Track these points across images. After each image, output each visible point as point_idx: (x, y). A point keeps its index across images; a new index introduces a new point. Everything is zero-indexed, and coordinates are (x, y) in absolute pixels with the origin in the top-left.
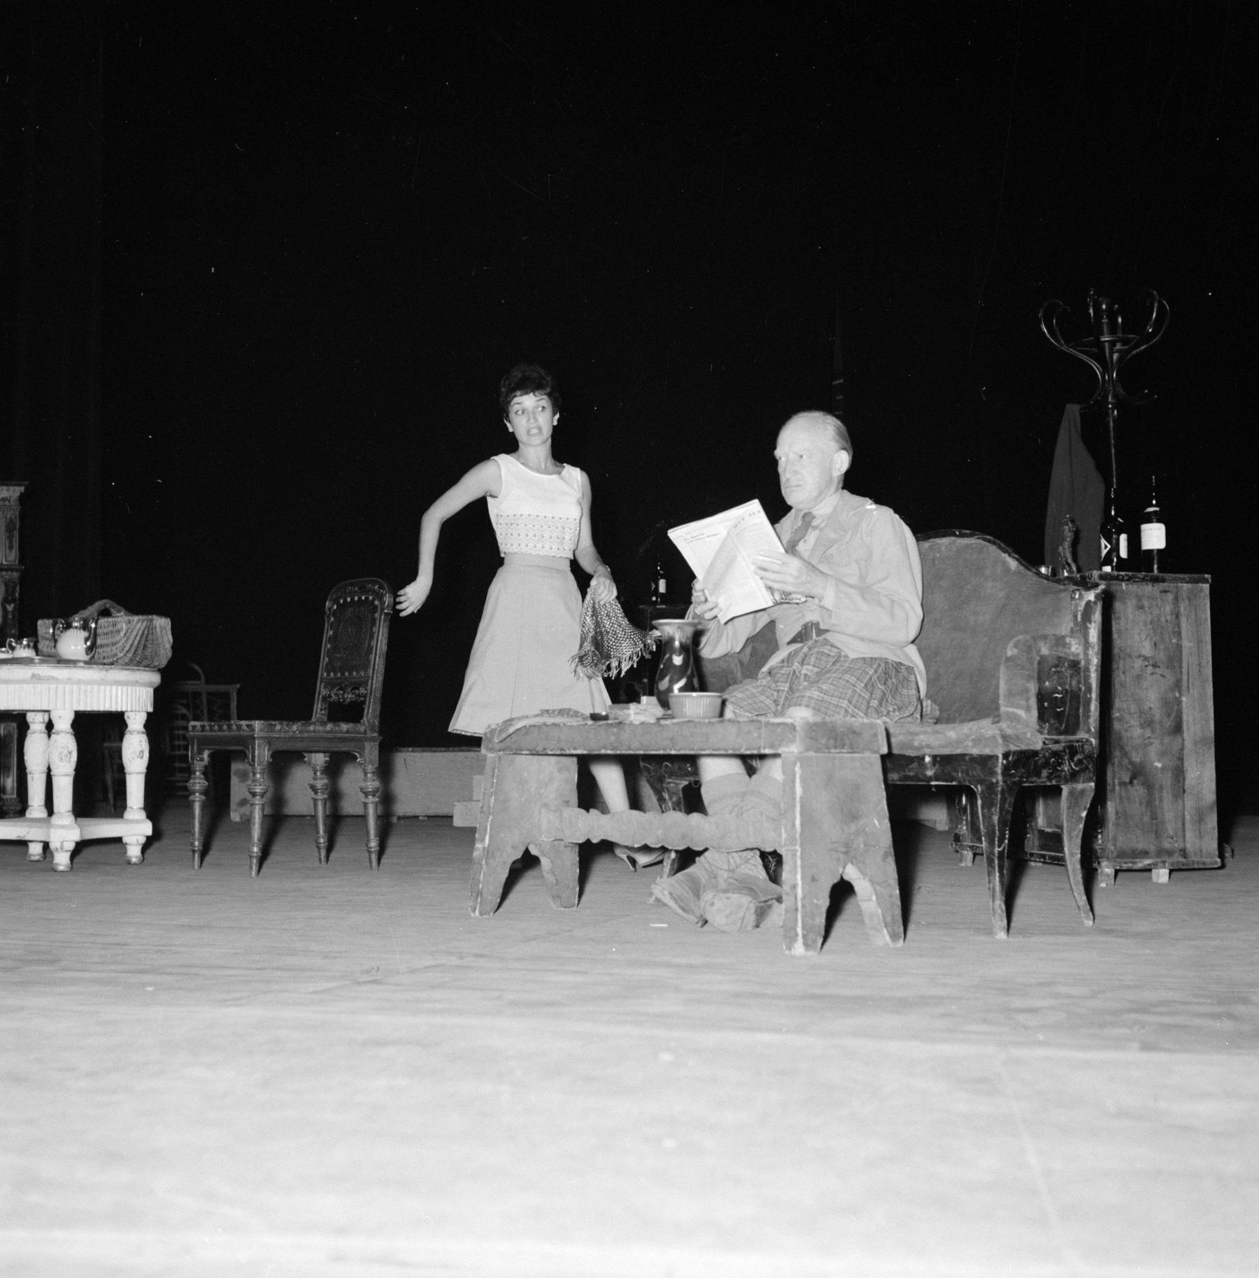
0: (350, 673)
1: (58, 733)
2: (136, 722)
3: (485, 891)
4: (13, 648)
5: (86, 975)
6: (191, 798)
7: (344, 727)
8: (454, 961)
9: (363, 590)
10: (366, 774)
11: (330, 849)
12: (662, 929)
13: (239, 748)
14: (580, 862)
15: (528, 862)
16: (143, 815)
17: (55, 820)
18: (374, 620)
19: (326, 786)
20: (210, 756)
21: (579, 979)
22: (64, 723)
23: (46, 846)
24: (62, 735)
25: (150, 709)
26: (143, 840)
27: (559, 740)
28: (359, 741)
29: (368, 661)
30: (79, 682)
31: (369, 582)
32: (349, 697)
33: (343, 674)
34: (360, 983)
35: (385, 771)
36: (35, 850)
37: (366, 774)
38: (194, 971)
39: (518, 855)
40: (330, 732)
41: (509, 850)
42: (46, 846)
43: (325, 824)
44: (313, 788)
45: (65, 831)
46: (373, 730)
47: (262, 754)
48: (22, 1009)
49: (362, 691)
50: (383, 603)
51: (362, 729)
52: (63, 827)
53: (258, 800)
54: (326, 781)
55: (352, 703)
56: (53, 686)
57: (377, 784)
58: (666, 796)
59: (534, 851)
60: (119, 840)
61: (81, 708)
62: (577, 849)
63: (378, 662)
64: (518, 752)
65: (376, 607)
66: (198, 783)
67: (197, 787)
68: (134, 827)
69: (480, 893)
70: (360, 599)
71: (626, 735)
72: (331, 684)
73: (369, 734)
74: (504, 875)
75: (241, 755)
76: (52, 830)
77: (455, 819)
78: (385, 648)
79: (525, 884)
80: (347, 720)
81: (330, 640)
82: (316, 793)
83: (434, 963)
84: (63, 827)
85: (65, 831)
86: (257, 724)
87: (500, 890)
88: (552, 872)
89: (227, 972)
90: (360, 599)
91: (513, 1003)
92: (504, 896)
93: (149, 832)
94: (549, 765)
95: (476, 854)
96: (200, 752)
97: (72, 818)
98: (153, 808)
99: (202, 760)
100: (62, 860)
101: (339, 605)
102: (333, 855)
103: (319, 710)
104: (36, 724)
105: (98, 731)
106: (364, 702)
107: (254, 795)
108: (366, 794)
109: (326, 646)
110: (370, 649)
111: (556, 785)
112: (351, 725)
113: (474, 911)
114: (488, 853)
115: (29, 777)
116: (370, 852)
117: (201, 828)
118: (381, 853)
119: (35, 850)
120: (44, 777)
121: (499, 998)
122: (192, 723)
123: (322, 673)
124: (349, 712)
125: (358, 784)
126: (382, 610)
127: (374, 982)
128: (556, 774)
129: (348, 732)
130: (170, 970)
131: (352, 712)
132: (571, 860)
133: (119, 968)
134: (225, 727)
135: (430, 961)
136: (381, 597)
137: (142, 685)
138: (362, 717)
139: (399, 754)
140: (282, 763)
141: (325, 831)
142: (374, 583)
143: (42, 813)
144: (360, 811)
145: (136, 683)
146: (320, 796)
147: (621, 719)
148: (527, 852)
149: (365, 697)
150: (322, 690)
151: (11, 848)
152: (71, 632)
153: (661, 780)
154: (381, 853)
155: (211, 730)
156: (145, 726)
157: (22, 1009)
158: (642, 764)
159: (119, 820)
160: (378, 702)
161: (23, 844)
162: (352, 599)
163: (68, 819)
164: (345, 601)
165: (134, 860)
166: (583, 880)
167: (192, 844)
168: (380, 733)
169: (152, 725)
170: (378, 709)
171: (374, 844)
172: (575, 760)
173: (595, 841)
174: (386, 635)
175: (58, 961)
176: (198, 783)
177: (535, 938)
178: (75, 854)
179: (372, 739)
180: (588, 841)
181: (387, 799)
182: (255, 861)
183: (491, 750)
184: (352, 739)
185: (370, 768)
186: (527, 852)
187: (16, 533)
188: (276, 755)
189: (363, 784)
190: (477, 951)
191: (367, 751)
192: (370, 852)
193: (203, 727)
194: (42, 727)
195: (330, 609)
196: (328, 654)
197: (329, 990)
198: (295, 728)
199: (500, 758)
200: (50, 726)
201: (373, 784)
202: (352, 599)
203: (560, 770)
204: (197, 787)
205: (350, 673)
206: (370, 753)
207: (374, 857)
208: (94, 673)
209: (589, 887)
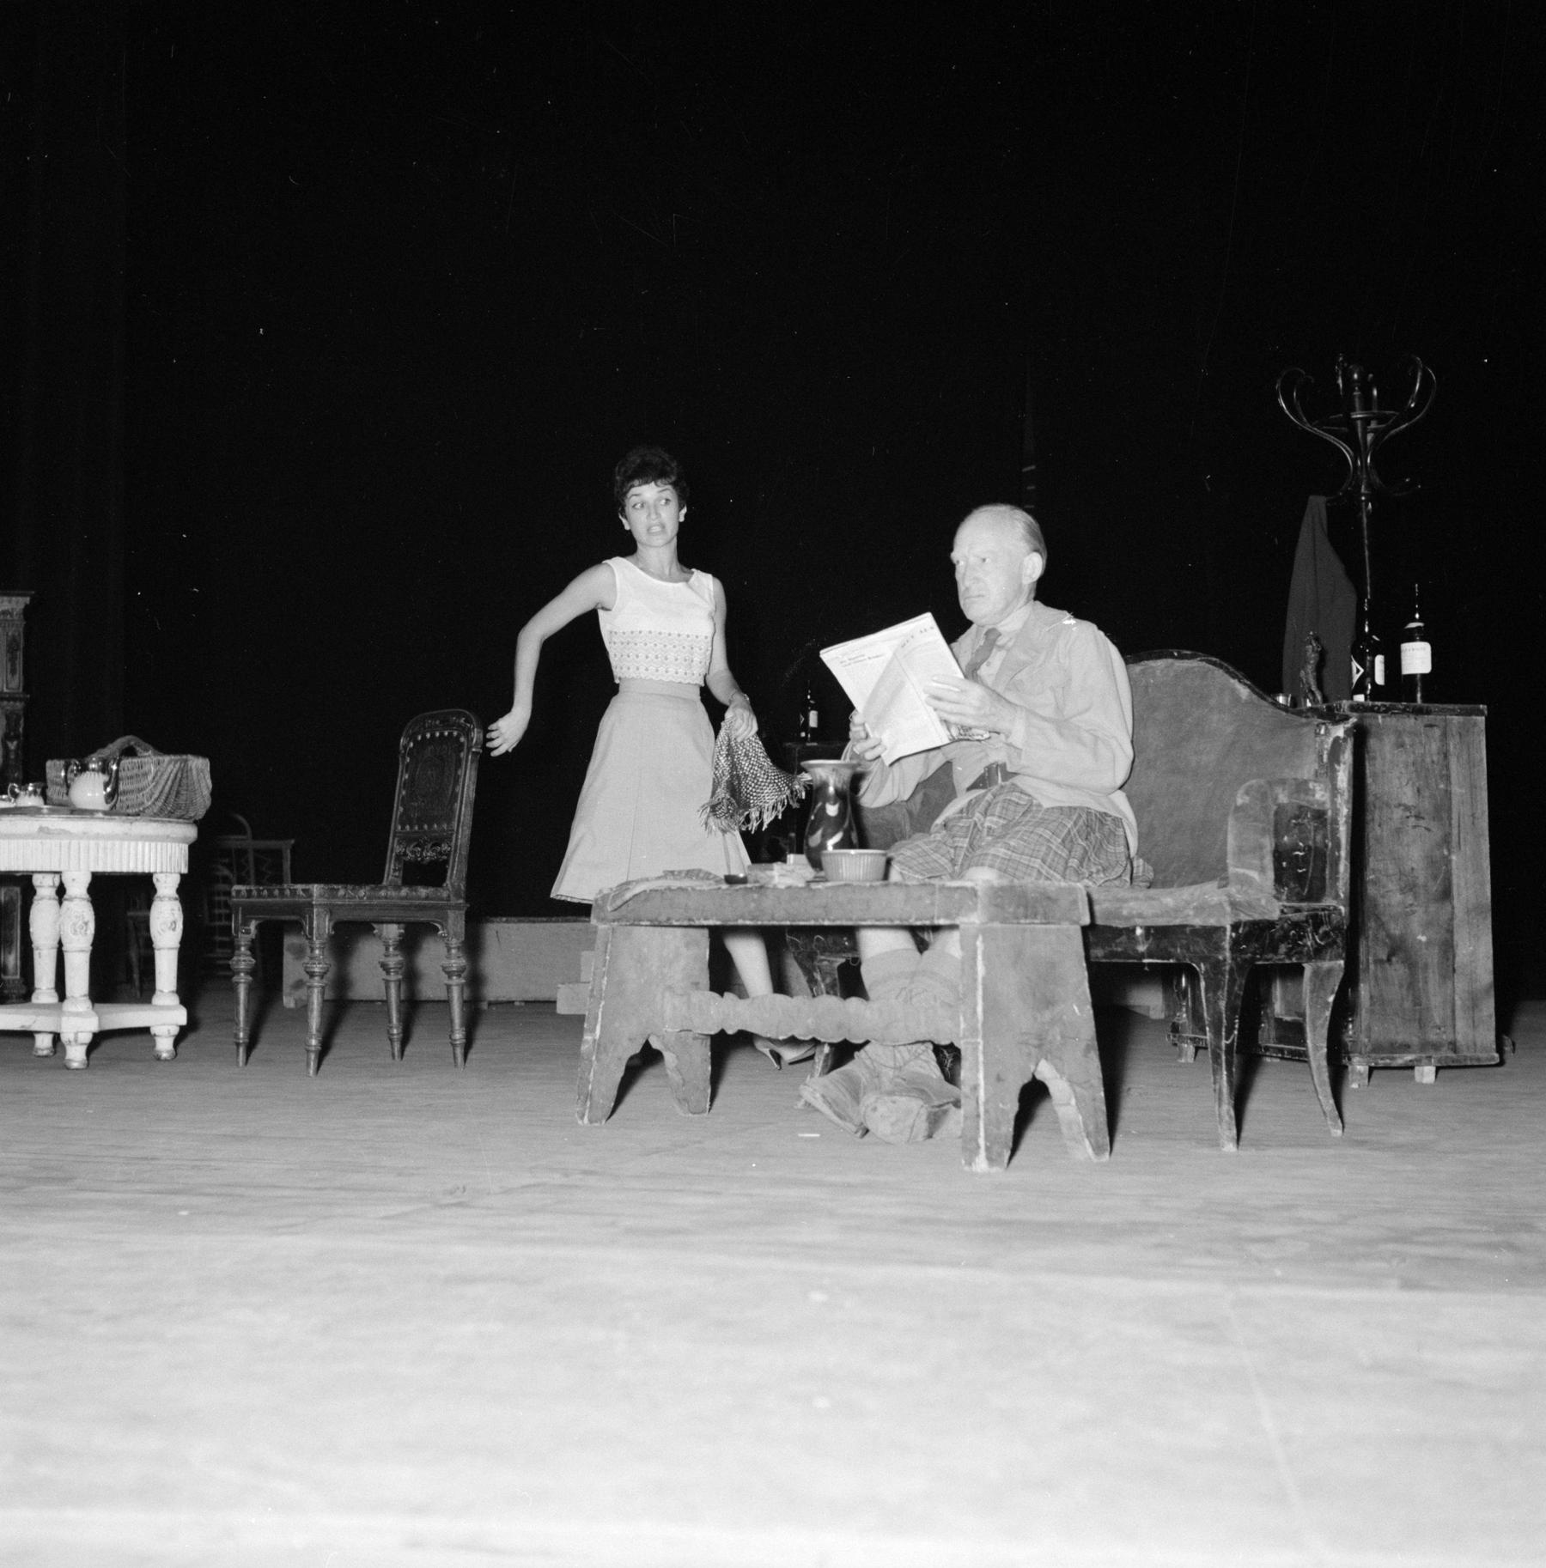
0: (430, 826)
1: (71, 899)
2: (167, 886)
3: (595, 1093)
4: (16, 796)
5: (106, 1196)
6: (235, 979)
7: (423, 891)
8: (557, 1179)
9: (446, 724)
10: (449, 950)
11: (405, 1041)
12: (812, 1139)
13: (294, 918)
14: (713, 1057)
15: (648, 1057)
16: (175, 1000)
17: (67, 1006)
18: (459, 761)
19: (400, 965)
20: (258, 927)
21: (711, 1201)
22: (78, 887)
23: (57, 1038)
24: (76, 901)
25: (185, 870)
26: (175, 1031)
27: (687, 908)
28: (441, 910)
29: (452, 811)
30: (97, 837)
31: (453, 714)
32: (429, 855)
33: (421, 827)
34: (442, 1207)
35: (473, 946)
36: (43, 1043)
37: (449, 950)
38: (239, 1191)
39: (636, 1049)
40: (406, 898)
41: (625, 1043)
42: (57, 1038)
43: (399, 1011)
44: (384, 966)
45: (80, 1020)
46: (458, 896)
47: (322, 925)
48: (27, 1238)
49: (445, 847)
50: (470, 740)
51: (445, 895)
52: (78, 1014)
53: (316, 982)
54: (400, 958)
55: (433, 863)
56: (65, 842)
57: (463, 962)
58: (818, 976)
59: (655, 1044)
60: (146, 1031)
61: (100, 869)
62: (709, 1042)
63: (464, 812)
64: (636, 922)
65: (462, 745)
66: (243, 960)
67: (242, 966)
68: (164, 1015)
69: (589, 1096)
70: (442, 734)
71: (768, 902)
72: (406, 840)
73: (453, 901)
74: (619, 1073)
75: (296, 927)
76: (64, 1019)
77: (559, 1005)
78: (472, 795)
79: (645, 1085)
80: (426, 883)
81: (405, 785)
82: (388, 973)
83: (533, 1181)
84: (78, 1014)
85: (80, 1020)
86: (316, 889)
87: (614, 1093)
88: (678, 1070)
89: (279, 1193)
90: (442, 734)
91: (630, 1231)
92: (619, 1099)
93: (183, 1021)
94: (674, 938)
95: (584, 1048)
96: (246, 923)
97: (89, 1003)
98: (188, 992)
99: (248, 932)
100: (76, 1055)
101: (416, 742)
102: (409, 1049)
103: (391, 871)
104: (45, 888)
105: (120, 897)
106: (447, 862)
107: (312, 975)
108: (450, 974)
109: (400, 793)
110: (454, 796)
111: (682, 963)
112: (431, 890)
113: (582, 1117)
114: (599, 1046)
115: (36, 953)
116: (454, 1046)
117: (247, 1016)
118: (468, 1046)
119: (43, 1043)
120: (54, 953)
121: (613, 1224)
122: (236, 887)
123: (395, 826)
124: (428, 873)
125: (440, 962)
126: (469, 748)
127: (460, 1205)
128: (683, 950)
129: (427, 898)
130: (208, 1190)
131: (432, 874)
132: (701, 1055)
133: (147, 1187)
134: (276, 892)
135: (528, 1179)
136: (467, 733)
137: (175, 840)
138: (444, 880)
139: (490, 926)
140: (347, 936)
141: (399, 1020)
142: (459, 715)
143: (52, 998)
144: (442, 995)
145: (167, 838)
146: (393, 977)
147: (762, 882)
148: (647, 1045)
149: (448, 855)
150: (395, 847)
151: (13, 1041)
152: (87, 776)
153: (811, 957)
154: (468, 1046)
155: (259, 896)
156: (178, 891)
157: (27, 1238)
158: (788, 937)
159: (146, 1007)
160: (464, 861)
161: (29, 1035)
162: (433, 735)
163: (84, 1005)
164: (424, 737)
165: (164, 1055)
166: (716, 1079)
167: (236, 1036)
168: (467, 899)
169: (187, 890)
170: (465, 870)
171: (459, 1035)
172: (706, 932)
173: (730, 1032)
174: (474, 779)
175: (71, 1179)
176: (243, 960)
177: (657, 1151)
178: (92, 1047)
179: (457, 907)
180: (722, 1032)
181: (475, 980)
182: (313, 1056)
183: (603, 920)
184: (432, 907)
185: (454, 942)
186: (647, 1045)
187: (20, 654)
188: (340, 926)
189: (445, 962)
190: (586, 1167)
191: (450, 921)
192: (454, 1046)
193: (249, 892)
194: (52, 892)
195: (405, 747)
196: (403, 802)
197: (405, 1215)
198: (362, 893)
199: (613, 930)
200: (61, 891)
201: (457, 961)
202: (433, 735)
203: (687, 945)
204: (242, 966)
205: (430, 826)
206: (455, 924)
207: (459, 1051)
208: (115, 826)
209: (724, 1088)
